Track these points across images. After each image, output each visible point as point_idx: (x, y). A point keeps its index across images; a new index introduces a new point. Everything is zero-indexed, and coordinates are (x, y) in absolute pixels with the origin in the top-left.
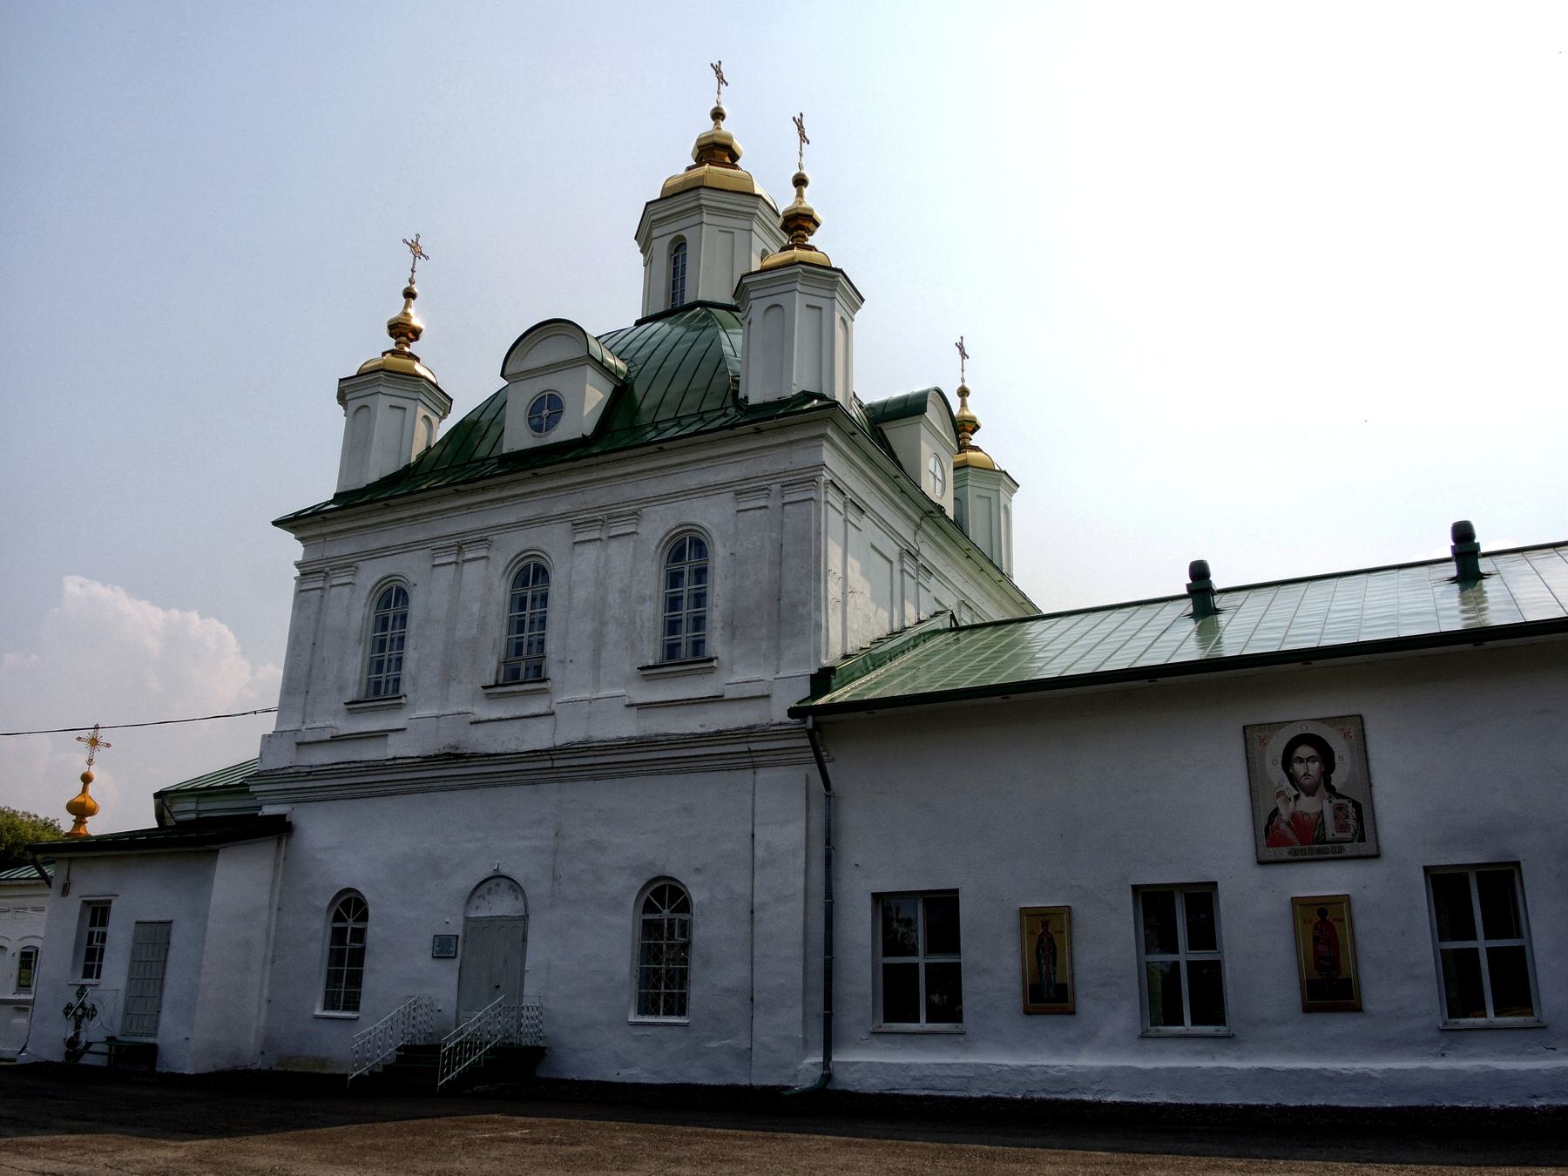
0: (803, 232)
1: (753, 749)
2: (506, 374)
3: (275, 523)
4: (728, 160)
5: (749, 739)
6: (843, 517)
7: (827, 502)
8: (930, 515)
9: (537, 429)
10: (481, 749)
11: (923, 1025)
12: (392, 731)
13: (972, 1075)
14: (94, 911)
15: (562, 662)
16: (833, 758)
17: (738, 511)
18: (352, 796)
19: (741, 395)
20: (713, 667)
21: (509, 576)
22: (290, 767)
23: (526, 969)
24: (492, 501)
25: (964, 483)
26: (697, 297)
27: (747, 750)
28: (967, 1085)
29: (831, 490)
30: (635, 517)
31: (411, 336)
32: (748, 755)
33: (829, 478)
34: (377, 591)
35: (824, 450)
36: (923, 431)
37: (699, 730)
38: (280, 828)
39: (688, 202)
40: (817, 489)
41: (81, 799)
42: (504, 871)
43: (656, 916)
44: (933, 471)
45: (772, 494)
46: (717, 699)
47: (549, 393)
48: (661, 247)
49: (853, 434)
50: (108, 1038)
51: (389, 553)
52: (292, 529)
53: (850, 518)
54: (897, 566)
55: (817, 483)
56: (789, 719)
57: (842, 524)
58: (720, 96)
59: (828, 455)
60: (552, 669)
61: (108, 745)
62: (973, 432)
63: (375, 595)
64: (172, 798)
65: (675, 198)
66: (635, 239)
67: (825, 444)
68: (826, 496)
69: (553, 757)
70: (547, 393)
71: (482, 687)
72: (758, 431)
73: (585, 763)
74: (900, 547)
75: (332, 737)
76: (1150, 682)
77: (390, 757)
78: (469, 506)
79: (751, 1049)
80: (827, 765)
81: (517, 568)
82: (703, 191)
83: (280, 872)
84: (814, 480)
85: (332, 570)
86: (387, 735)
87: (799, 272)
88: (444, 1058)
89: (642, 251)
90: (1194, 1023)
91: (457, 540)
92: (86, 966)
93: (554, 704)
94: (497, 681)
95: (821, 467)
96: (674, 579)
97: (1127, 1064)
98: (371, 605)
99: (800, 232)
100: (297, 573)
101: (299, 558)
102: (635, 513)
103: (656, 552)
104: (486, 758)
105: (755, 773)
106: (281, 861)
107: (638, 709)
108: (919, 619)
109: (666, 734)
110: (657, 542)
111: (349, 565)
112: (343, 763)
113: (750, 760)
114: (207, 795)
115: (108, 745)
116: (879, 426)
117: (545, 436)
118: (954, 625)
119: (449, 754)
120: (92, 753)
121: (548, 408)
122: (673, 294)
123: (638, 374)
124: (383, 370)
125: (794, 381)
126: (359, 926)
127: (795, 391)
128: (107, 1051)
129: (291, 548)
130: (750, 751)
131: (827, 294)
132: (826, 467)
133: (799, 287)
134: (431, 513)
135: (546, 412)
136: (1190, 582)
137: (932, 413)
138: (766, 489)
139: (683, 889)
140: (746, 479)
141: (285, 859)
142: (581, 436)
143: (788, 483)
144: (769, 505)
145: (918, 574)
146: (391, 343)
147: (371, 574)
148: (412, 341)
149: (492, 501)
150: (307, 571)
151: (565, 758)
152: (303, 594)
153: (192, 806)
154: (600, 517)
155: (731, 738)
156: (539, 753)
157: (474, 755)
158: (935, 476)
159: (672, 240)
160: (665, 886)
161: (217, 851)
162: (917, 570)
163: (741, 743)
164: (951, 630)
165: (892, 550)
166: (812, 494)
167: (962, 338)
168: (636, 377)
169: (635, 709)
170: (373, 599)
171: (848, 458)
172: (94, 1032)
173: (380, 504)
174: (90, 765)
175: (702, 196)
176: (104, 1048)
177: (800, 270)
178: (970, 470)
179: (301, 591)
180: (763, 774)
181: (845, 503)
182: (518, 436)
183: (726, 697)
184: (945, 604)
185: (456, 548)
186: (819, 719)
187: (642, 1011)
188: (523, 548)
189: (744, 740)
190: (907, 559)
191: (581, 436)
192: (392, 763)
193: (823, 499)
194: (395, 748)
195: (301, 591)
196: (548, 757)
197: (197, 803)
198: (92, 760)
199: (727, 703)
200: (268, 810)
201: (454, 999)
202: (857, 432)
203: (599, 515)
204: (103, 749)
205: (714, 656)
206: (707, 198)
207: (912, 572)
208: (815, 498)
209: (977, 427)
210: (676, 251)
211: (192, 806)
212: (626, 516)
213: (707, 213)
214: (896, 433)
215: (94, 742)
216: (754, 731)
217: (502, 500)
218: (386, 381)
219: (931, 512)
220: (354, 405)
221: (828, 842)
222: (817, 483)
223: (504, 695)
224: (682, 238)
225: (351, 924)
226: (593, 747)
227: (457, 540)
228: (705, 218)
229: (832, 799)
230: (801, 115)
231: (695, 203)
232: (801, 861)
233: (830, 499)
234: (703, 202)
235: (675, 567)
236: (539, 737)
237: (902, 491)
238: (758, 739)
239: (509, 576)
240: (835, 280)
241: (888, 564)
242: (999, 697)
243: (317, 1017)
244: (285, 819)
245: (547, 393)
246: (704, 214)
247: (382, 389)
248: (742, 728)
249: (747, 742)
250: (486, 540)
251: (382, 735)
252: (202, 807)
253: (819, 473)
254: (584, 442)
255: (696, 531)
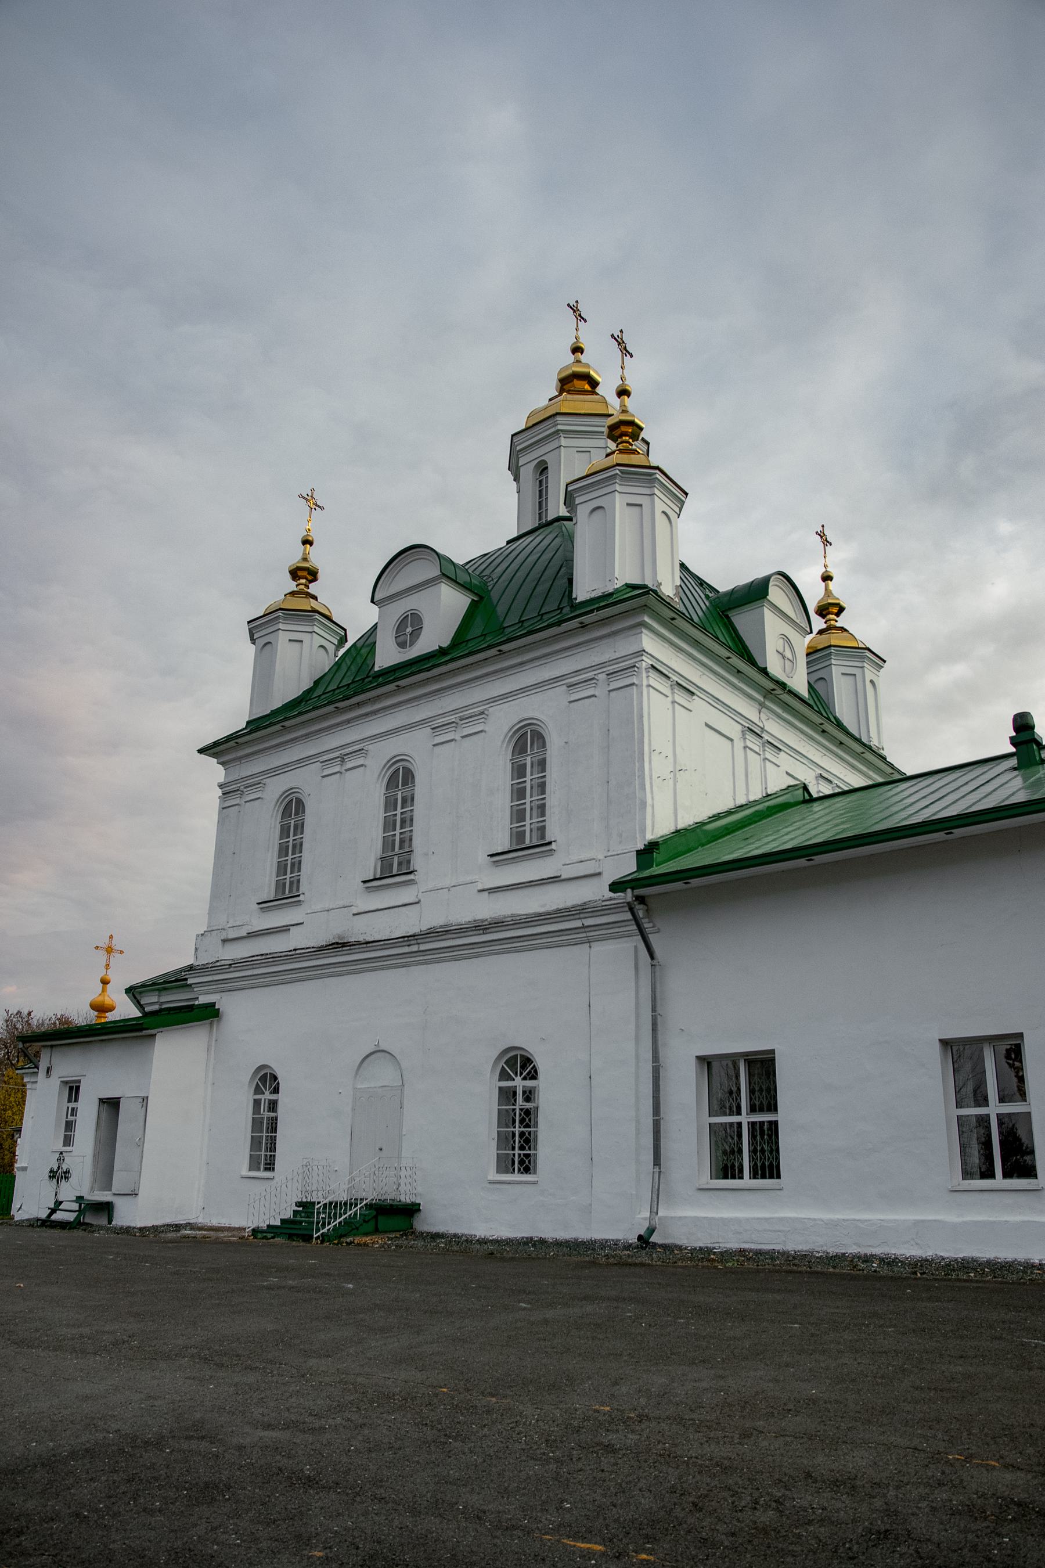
0: (627, 438)
1: (586, 924)
2: (375, 601)
3: (201, 751)
4: (587, 387)
5: (582, 916)
6: (670, 699)
7: (649, 686)
8: (773, 692)
9: (402, 645)
10: (361, 939)
11: (747, 1181)
12: (293, 925)
13: (789, 1229)
14: (71, 1088)
15: (426, 854)
16: (659, 929)
17: (570, 702)
18: (250, 986)
19: (574, 596)
20: (552, 850)
21: (382, 781)
22: (218, 961)
23: (404, 1133)
24: (367, 715)
25: (828, 663)
26: (558, 513)
27: (581, 925)
28: (784, 1239)
29: (653, 674)
30: (483, 716)
31: (310, 578)
32: (583, 930)
33: (651, 663)
34: (281, 803)
35: (644, 636)
36: (768, 614)
37: (542, 910)
38: (210, 1013)
39: (547, 430)
40: (639, 673)
41: (101, 999)
42: (383, 1047)
43: (509, 1084)
44: (781, 651)
45: (600, 683)
46: (555, 880)
47: (412, 612)
48: (528, 472)
49: (673, 619)
50: (78, 1197)
51: (289, 769)
52: (214, 755)
53: (677, 700)
54: (739, 744)
55: (638, 668)
56: (612, 895)
57: (670, 706)
58: (579, 333)
59: (648, 642)
60: (418, 862)
61: (122, 952)
62: (838, 614)
63: (279, 806)
64: (141, 993)
65: (535, 427)
66: (509, 469)
67: (644, 630)
68: (648, 680)
69: (419, 941)
70: (409, 613)
71: (362, 882)
72: (583, 626)
73: (446, 945)
74: (742, 725)
75: (248, 933)
76: (947, 834)
77: (292, 949)
78: (348, 721)
79: (591, 1205)
80: (650, 936)
81: (388, 774)
82: (559, 418)
83: (213, 1053)
84: (635, 666)
85: (246, 788)
86: (289, 929)
87: (617, 474)
88: (319, 1213)
89: (515, 480)
90: (1006, 1175)
91: (340, 752)
92: (65, 1136)
93: (420, 894)
94: (375, 875)
95: (641, 653)
96: (519, 771)
97: (1031, 1219)
98: (276, 816)
99: (624, 438)
100: (219, 792)
101: (222, 780)
102: (482, 713)
103: (501, 747)
104: (365, 946)
105: (590, 947)
106: (214, 1042)
107: (489, 893)
108: (767, 793)
109: (513, 916)
110: (502, 738)
111: (255, 783)
112: (257, 956)
113: (584, 935)
114: (165, 989)
115: (122, 952)
116: (726, 613)
117: (409, 651)
118: (807, 797)
119: (337, 943)
120: (109, 959)
121: (411, 626)
122: (539, 514)
123: (493, 587)
124: (281, 609)
125: (616, 575)
126: (273, 1097)
127: (618, 584)
128: (77, 1209)
129: (214, 771)
130: (584, 927)
131: (647, 491)
132: (647, 653)
133: (618, 487)
134: (320, 730)
135: (409, 630)
136: (1014, 734)
137: (776, 594)
138: (593, 679)
139: (531, 1058)
140: (576, 672)
141: (216, 1040)
142: (438, 648)
143: (612, 671)
144: (597, 694)
145: (764, 750)
146: (292, 586)
147: (275, 788)
148: (311, 582)
149: (367, 715)
150: (228, 791)
151: (431, 942)
152: (225, 810)
153: (155, 999)
154: (454, 720)
155: (569, 915)
156: (406, 939)
157: (359, 943)
158: (784, 657)
159: (536, 466)
160: (517, 1055)
161: (154, 1036)
162: (764, 746)
163: (576, 919)
164: (805, 802)
165: (733, 730)
166: (635, 680)
167: (823, 526)
168: (492, 589)
169: (486, 893)
170: (278, 811)
171: (672, 644)
172: (68, 1192)
173: (278, 727)
174: (107, 969)
175: (558, 422)
176: (75, 1206)
177: (618, 472)
178: (833, 650)
179: (223, 808)
180: (597, 947)
181: (671, 686)
182: (387, 655)
183: (563, 877)
184: (799, 778)
185: (339, 759)
186: (637, 892)
187: (500, 1170)
188: (393, 754)
189: (578, 916)
190: (749, 736)
191: (438, 648)
192: (293, 953)
193: (645, 683)
194: (296, 940)
195: (223, 808)
196: (415, 942)
197: (159, 996)
198: (108, 965)
199: (564, 883)
200: (203, 999)
201: (347, 1160)
202: (676, 616)
203: (452, 718)
204: (117, 955)
205: (553, 840)
206: (563, 423)
207: (757, 749)
208: (636, 682)
209: (841, 609)
210: (541, 473)
211: (155, 999)
212: (475, 716)
213: (565, 437)
214: (741, 620)
215: (109, 950)
216: (587, 907)
217: (375, 712)
218: (285, 619)
219: (773, 690)
220: (261, 642)
221: (654, 1009)
222: (638, 668)
223: (380, 888)
224: (544, 462)
225: (268, 1096)
226: (451, 930)
227: (340, 752)
228: (564, 442)
229: (658, 968)
230: (621, 331)
231: (553, 430)
232: (632, 1027)
233: (652, 682)
234: (560, 427)
235: (520, 760)
236: (408, 923)
237: (739, 671)
238: (590, 915)
239: (382, 781)
240: (654, 477)
241: (729, 742)
242: (803, 860)
243: (491, 1182)
244: (215, 1006)
245: (409, 613)
246: (562, 438)
247: (281, 626)
248: (578, 906)
249: (580, 918)
250: (362, 749)
251: (285, 929)
252: (163, 999)
253: (640, 659)
254: (442, 652)
255: (539, 725)
